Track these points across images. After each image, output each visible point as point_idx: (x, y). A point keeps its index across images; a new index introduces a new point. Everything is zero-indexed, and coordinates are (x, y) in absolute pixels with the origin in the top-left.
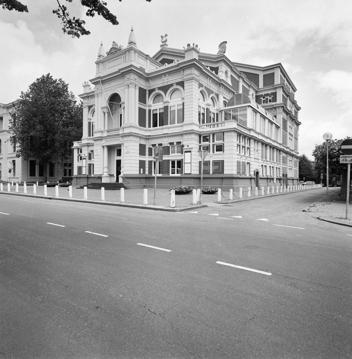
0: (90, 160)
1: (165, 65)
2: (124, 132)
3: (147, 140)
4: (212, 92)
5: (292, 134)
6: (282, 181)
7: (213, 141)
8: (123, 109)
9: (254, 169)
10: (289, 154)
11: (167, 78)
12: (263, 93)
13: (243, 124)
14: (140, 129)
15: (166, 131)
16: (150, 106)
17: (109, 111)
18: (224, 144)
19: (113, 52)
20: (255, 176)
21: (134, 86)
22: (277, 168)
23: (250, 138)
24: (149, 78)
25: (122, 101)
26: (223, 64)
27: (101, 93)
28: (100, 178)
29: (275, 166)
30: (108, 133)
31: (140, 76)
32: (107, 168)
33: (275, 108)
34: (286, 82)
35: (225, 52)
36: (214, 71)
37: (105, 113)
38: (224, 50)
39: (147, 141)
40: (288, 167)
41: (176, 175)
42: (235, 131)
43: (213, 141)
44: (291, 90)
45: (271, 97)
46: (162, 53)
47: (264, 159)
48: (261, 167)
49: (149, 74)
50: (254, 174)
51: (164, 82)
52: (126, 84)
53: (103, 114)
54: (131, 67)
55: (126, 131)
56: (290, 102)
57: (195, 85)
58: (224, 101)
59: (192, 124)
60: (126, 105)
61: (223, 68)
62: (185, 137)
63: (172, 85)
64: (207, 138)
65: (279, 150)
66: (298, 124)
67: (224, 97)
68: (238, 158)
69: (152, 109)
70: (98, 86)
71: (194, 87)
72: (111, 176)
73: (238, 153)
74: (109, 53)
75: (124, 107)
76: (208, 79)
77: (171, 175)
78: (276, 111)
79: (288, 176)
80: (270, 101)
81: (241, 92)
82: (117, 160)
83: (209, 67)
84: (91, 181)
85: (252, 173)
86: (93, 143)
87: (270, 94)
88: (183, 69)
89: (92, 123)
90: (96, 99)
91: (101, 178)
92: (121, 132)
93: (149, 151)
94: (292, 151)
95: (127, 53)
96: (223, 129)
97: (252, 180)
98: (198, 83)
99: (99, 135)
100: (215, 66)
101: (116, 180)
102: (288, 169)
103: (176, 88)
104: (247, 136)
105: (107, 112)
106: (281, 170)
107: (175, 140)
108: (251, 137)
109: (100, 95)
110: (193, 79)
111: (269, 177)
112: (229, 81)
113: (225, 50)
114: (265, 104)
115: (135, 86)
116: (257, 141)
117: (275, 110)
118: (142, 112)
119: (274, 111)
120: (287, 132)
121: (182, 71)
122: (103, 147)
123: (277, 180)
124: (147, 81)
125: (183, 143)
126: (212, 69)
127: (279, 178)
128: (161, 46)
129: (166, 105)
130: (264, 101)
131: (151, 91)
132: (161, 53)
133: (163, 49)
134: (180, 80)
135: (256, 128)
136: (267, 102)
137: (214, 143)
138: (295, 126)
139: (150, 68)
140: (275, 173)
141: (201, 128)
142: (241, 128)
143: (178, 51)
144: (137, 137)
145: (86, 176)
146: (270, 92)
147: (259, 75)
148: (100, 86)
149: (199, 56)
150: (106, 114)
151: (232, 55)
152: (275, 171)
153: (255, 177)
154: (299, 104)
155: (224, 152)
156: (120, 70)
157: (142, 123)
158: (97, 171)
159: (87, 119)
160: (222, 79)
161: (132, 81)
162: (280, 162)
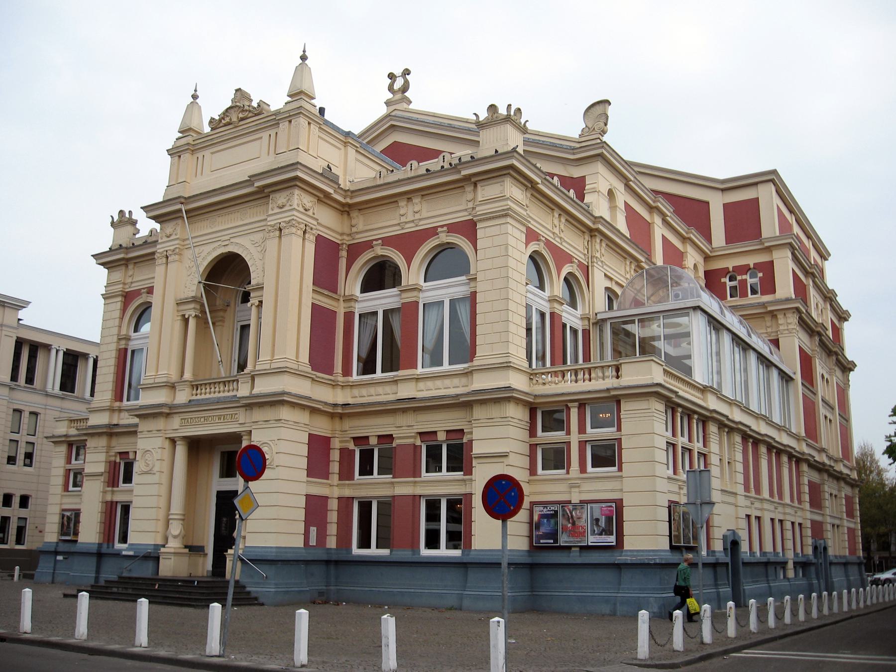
0: (113, 486)
1: (409, 165)
2: (256, 391)
3: (337, 420)
4: (569, 259)
5: (831, 402)
6: (813, 569)
7: (582, 429)
8: (254, 309)
9: (724, 531)
10: (827, 471)
11: (416, 210)
12: (730, 264)
13: (680, 366)
14: (313, 379)
15: (406, 391)
16: (350, 299)
17: (203, 312)
18: (619, 440)
19: (234, 119)
20: (726, 556)
21: (300, 233)
22: (793, 523)
23: (706, 419)
24: (350, 206)
26: (600, 168)
27: (178, 252)
28: (152, 557)
29: (788, 517)
30: (194, 392)
31: (324, 198)
32: (183, 520)
33: (773, 315)
34: (796, 229)
35: (604, 132)
36: (572, 191)
37: (186, 321)
38: (602, 124)
39: (337, 425)
40: (829, 520)
41: (443, 552)
42: (657, 395)
43: (582, 429)
44: (813, 254)
45: (756, 277)
46: (393, 126)
47: (753, 494)
48: (744, 524)
49: (353, 192)
50: (725, 549)
51: (403, 219)
52: (272, 223)
53: (178, 325)
54: (296, 169)
55: (264, 386)
56: (817, 296)
57: (515, 235)
58: (607, 289)
59: (507, 366)
60: (268, 297)
61: (600, 180)
62: (479, 413)
63: (432, 232)
64: (556, 416)
65: (797, 459)
66: (846, 367)
67: (606, 275)
68: (670, 492)
69: (359, 308)
70: (169, 228)
71: (512, 241)
72: (195, 550)
73: (670, 472)
74: (220, 120)
75: (261, 302)
76: (556, 215)
77: (356, 551)
78: (778, 325)
79: (831, 552)
80: (754, 292)
81: (659, 260)
83: (556, 178)
84: (110, 573)
85: (718, 546)
86: (136, 425)
87: (752, 266)
88: (473, 181)
89: (133, 352)
90: (159, 270)
91: (157, 559)
92: (243, 390)
93: (341, 462)
94: (836, 461)
95: (284, 125)
96: (615, 389)
97: (849, 567)
98: (524, 230)
99: (159, 397)
100: (575, 172)
101: (210, 569)
102: (829, 527)
103: (448, 243)
104: (695, 412)
105: (196, 316)
106: (809, 532)
107: (440, 424)
108: (707, 414)
109: (177, 257)
110: (506, 215)
111: (773, 559)
112: (622, 225)
113: (606, 124)
114: (738, 301)
115: (305, 232)
116: (727, 427)
117: (774, 321)
118: (322, 320)
119: (768, 324)
120: (815, 394)
121: (469, 189)
122: (173, 441)
123: (798, 568)
125: (471, 433)
126: (568, 182)
127: (803, 560)
128: (388, 103)
129: (409, 297)
130: (733, 288)
131: (355, 251)
132: (388, 124)
133: (393, 114)
134: (464, 217)
135: (720, 384)
136: (744, 295)
137: (584, 437)
138: (838, 373)
139: (357, 172)
140: (789, 544)
141: (534, 381)
142: (676, 384)
143: (431, 119)
144: (303, 407)
145: (94, 549)
146: (751, 261)
147: (708, 203)
148: (180, 230)
149: (526, 142)
150: (192, 323)
151: (623, 140)
152: (789, 535)
153: (728, 560)
154: (843, 301)
155: (620, 469)
156: (253, 178)
157: (321, 358)
158: (142, 533)
159: (115, 339)
160: (601, 217)
161: (295, 213)
162: (800, 502)
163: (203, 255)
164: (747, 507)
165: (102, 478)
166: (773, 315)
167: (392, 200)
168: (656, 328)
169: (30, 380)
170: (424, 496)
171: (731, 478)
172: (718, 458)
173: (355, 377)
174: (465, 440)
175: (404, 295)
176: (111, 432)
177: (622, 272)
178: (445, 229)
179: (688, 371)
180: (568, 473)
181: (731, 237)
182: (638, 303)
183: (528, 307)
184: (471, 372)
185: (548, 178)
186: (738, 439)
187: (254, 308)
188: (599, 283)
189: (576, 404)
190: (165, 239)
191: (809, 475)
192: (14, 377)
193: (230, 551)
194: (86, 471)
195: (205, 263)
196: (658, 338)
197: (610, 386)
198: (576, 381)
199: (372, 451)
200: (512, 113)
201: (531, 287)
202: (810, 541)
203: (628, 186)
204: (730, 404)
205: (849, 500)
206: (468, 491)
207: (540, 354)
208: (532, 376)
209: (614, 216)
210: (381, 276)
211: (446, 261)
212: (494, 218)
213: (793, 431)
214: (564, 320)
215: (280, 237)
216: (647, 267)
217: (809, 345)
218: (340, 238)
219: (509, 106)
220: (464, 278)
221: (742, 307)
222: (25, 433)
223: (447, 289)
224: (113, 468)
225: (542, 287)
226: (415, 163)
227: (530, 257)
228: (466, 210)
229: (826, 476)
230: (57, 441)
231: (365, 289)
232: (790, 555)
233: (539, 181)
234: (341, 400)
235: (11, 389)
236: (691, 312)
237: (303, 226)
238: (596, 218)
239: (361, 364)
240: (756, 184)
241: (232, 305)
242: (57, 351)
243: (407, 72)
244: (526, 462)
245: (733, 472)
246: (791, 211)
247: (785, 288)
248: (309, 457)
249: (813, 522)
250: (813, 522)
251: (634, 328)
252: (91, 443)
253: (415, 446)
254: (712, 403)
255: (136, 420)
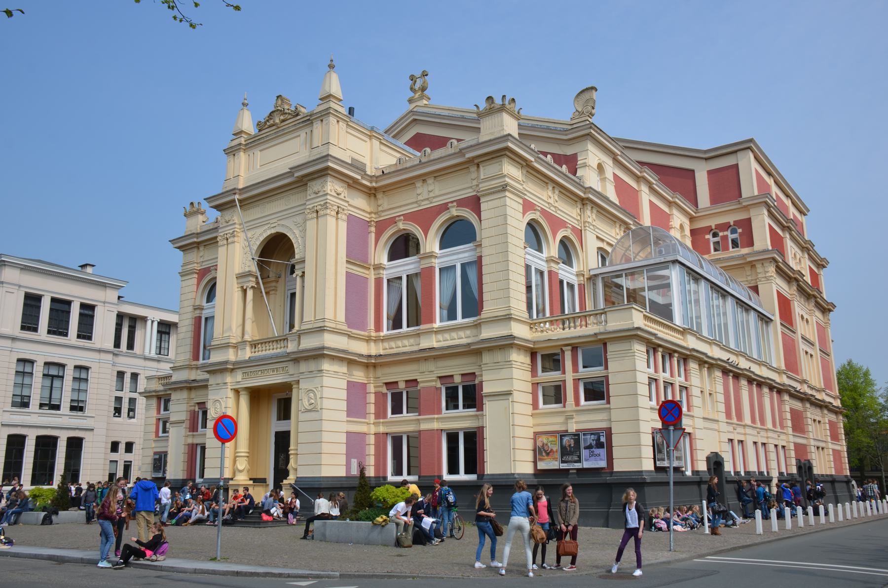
4: (563, 224)
5: (812, 339)
8: (298, 279)
9: (707, 453)
12: (713, 223)
13: (664, 312)
15: (432, 342)
16: (378, 267)
18: (607, 377)
19: (277, 121)
21: (334, 213)
22: (776, 446)
23: (686, 357)
24: (375, 189)
25: (297, 256)
26: (591, 147)
29: (770, 441)
31: (353, 184)
33: (752, 265)
34: (775, 190)
36: (564, 166)
37: (245, 291)
40: (812, 442)
43: (575, 369)
44: (792, 211)
46: (415, 120)
47: (735, 420)
48: (727, 447)
51: (420, 198)
52: (310, 206)
55: (308, 343)
57: (513, 205)
60: (309, 268)
62: (486, 358)
63: (444, 207)
64: (556, 357)
67: (598, 237)
69: (385, 275)
70: (228, 215)
74: (265, 123)
75: (304, 273)
76: (551, 188)
78: (757, 274)
81: (646, 221)
82: (277, 433)
83: (549, 156)
85: (702, 466)
86: (207, 380)
88: (476, 162)
89: (206, 319)
90: (222, 251)
92: (291, 347)
96: (601, 333)
98: (521, 201)
99: (231, 356)
100: (569, 151)
102: (813, 449)
103: (458, 216)
104: (675, 351)
106: (793, 454)
107: (456, 369)
114: (721, 255)
115: (337, 213)
116: (707, 364)
118: (354, 285)
119: (748, 273)
121: (473, 169)
124: (372, 198)
125: (481, 375)
126: (559, 159)
129: (425, 264)
131: (381, 227)
134: (469, 193)
137: (578, 376)
138: (818, 314)
140: (774, 465)
144: (341, 359)
146: (731, 219)
147: (693, 171)
148: (237, 216)
150: (250, 293)
152: (773, 456)
154: (821, 250)
155: (608, 402)
156: (294, 169)
160: (590, 188)
162: (782, 427)
163: (256, 236)
164: (729, 432)
165: (184, 425)
166: (752, 265)
167: (410, 183)
168: (642, 282)
169: (130, 346)
170: (445, 430)
171: (713, 407)
172: (699, 390)
173: (385, 332)
174: (477, 382)
175: (423, 262)
176: (190, 386)
177: (613, 234)
178: (455, 204)
179: (670, 317)
180: (564, 407)
181: (715, 199)
182: (628, 260)
183: (528, 268)
184: (480, 324)
185: (541, 156)
186: (718, 374)
187: (298, 279)
188: (592, 244)
189: (570, 348)
190: (225, 224)
191: (790, 404)
192: (117, 344)
193: (285, 482)
194: (171, 419)
195: (258, 243)
196: (643, 289)
197: (597, 331)
198: (564, 329)
199: (457, 387)
200: (507, 103)
201: (529, 250)
202: (794, 462)
203: (616, 161)
204: (710, 344)
205: (833, 425)
206: (480, 425)
207: (541, 307)
208: (532, 326)
209: (604, 187)
210: (404, 246)
211: (458, 233)
212: (494, 193)
213: (774, 365)
214: (561, 277)
215: (317, 218)
216: (634, 228)
217: (787, 289)
218: (368, 215)
219: (504, 96)
220: (471, 245)
221: (718, 260)
222: (128, 390)
223: (460, 254)
224: (193, 417)
225: (540, 249)
226: (428, 150)
227: (528, 224)
228: (471, 187)
229: (808, 405)
230: (148, 395)
231: (392, 256)
232: (775, 474)
233: (533, 159)
234: (373, 352)
235: (115, 355)
236: (671, 265)
237: (335, 208)
238: (586, 188)
239: (391, 322)
240: (736, 152)
241: (283, 276)
242: (153, 322)
243: (425, 74)
244: (529, 399)
245: (714, 402)
246: (769, 174)
247: (762, 240)
248: (349, 401)
249: (796, 445)
250: (796, 445)
251: (624, 282)
252: (174, 396)
253: (437, 388)
254: (691, 343)
255: (207, 376)
